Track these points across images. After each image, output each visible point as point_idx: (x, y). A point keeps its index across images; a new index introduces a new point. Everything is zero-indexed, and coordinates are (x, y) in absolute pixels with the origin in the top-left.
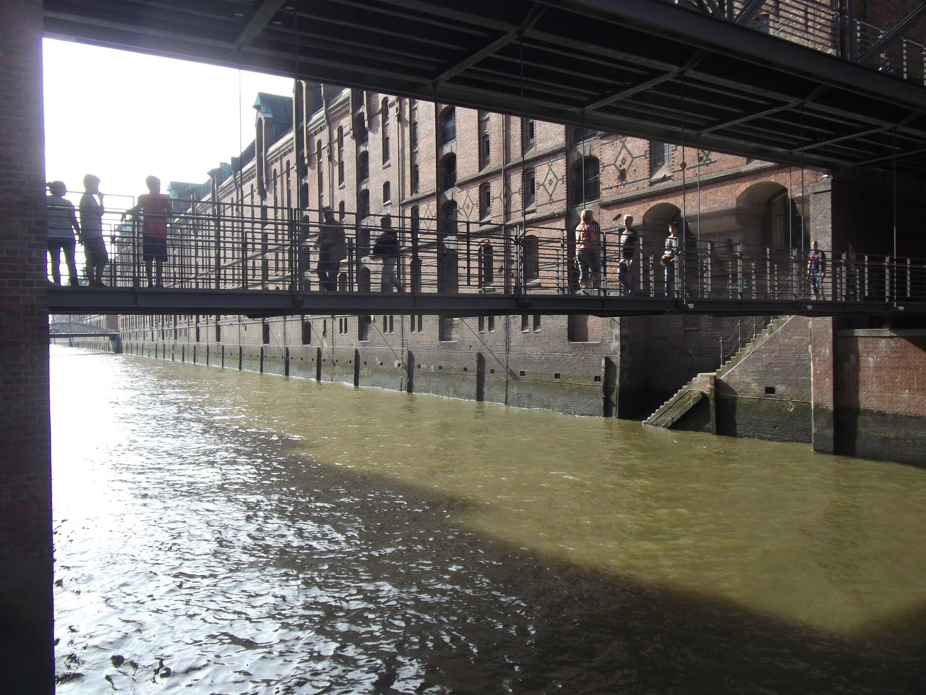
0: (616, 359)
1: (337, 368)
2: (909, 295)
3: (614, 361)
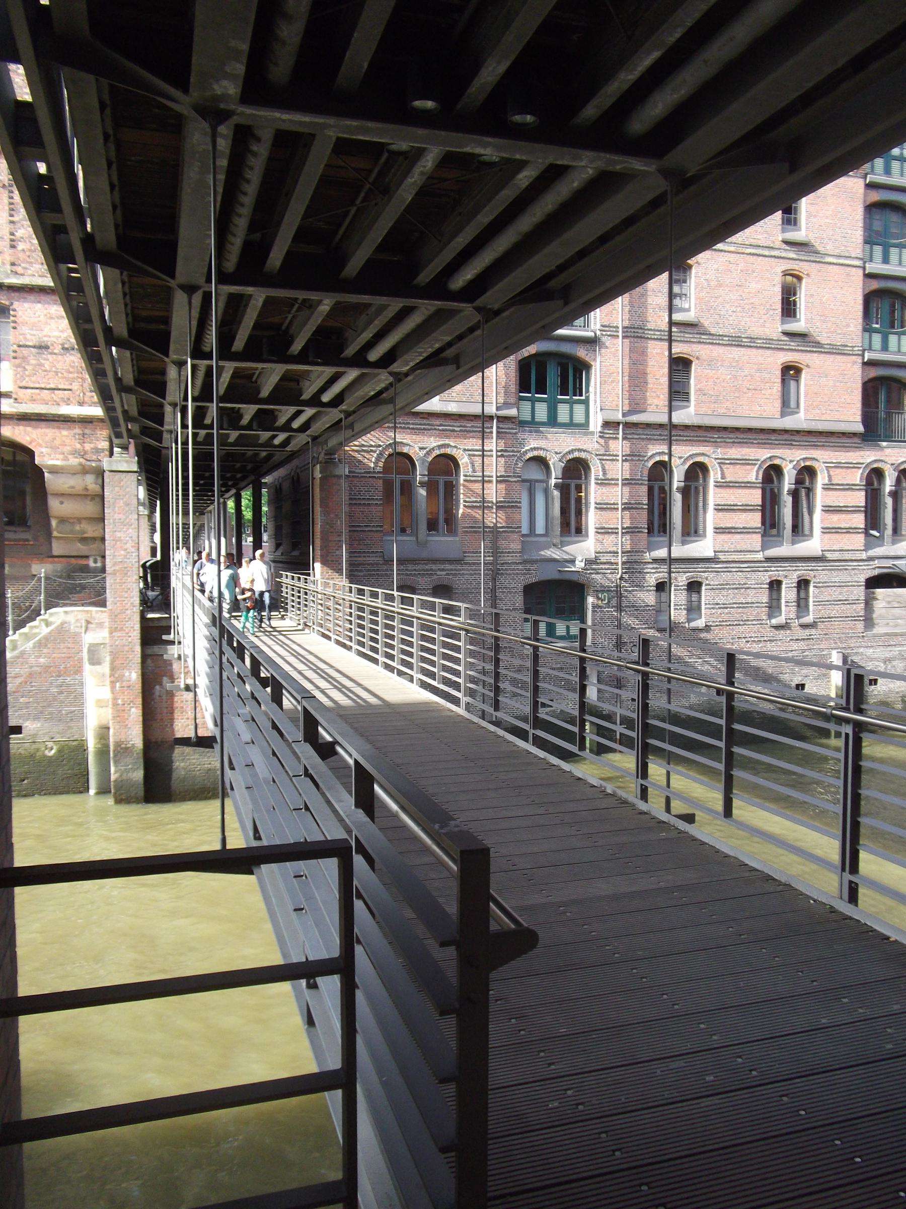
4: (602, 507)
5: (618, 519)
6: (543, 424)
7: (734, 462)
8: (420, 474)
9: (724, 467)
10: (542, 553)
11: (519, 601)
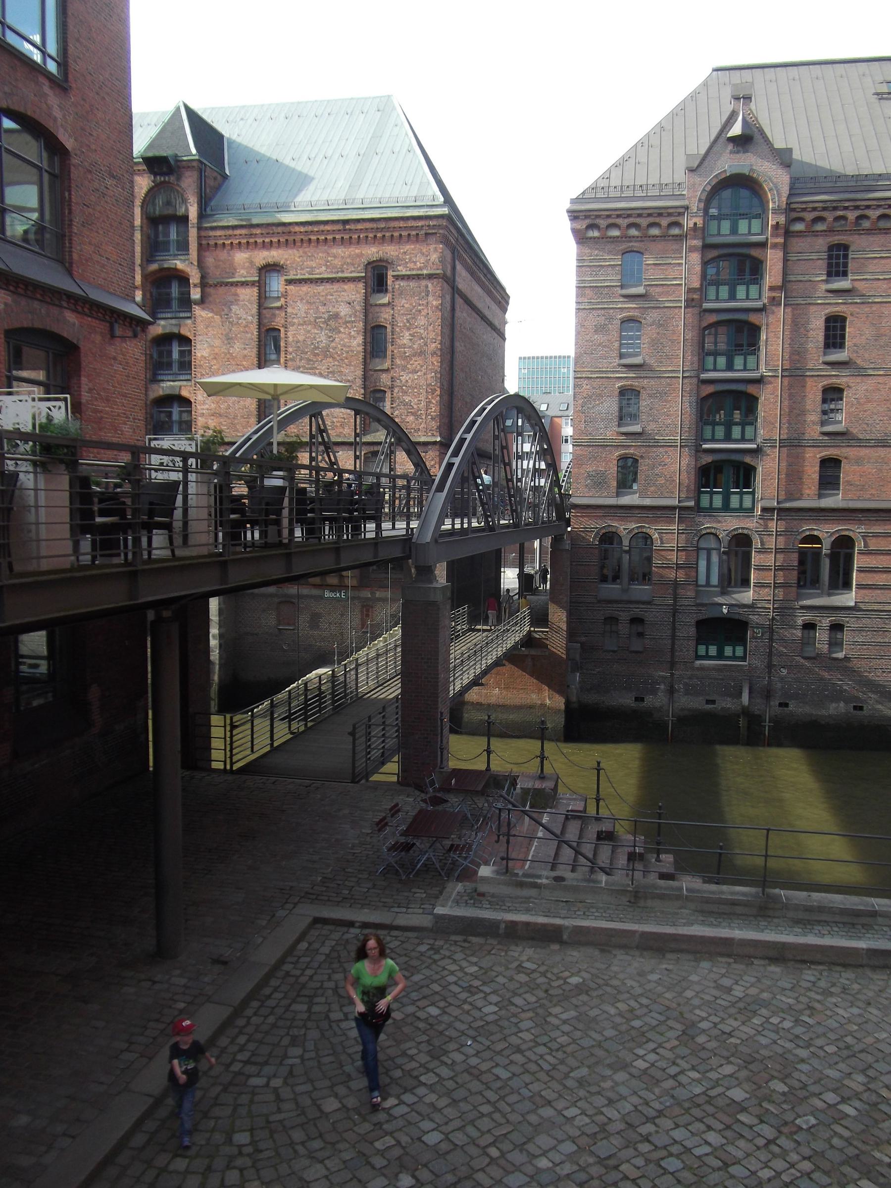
4: (760, 568)
5: (769, 578)
6: (717, 510)
7: (876, 535)
8: (626, 542)
9: (867, 539)
10: (716, 599)
11: (692, 631)
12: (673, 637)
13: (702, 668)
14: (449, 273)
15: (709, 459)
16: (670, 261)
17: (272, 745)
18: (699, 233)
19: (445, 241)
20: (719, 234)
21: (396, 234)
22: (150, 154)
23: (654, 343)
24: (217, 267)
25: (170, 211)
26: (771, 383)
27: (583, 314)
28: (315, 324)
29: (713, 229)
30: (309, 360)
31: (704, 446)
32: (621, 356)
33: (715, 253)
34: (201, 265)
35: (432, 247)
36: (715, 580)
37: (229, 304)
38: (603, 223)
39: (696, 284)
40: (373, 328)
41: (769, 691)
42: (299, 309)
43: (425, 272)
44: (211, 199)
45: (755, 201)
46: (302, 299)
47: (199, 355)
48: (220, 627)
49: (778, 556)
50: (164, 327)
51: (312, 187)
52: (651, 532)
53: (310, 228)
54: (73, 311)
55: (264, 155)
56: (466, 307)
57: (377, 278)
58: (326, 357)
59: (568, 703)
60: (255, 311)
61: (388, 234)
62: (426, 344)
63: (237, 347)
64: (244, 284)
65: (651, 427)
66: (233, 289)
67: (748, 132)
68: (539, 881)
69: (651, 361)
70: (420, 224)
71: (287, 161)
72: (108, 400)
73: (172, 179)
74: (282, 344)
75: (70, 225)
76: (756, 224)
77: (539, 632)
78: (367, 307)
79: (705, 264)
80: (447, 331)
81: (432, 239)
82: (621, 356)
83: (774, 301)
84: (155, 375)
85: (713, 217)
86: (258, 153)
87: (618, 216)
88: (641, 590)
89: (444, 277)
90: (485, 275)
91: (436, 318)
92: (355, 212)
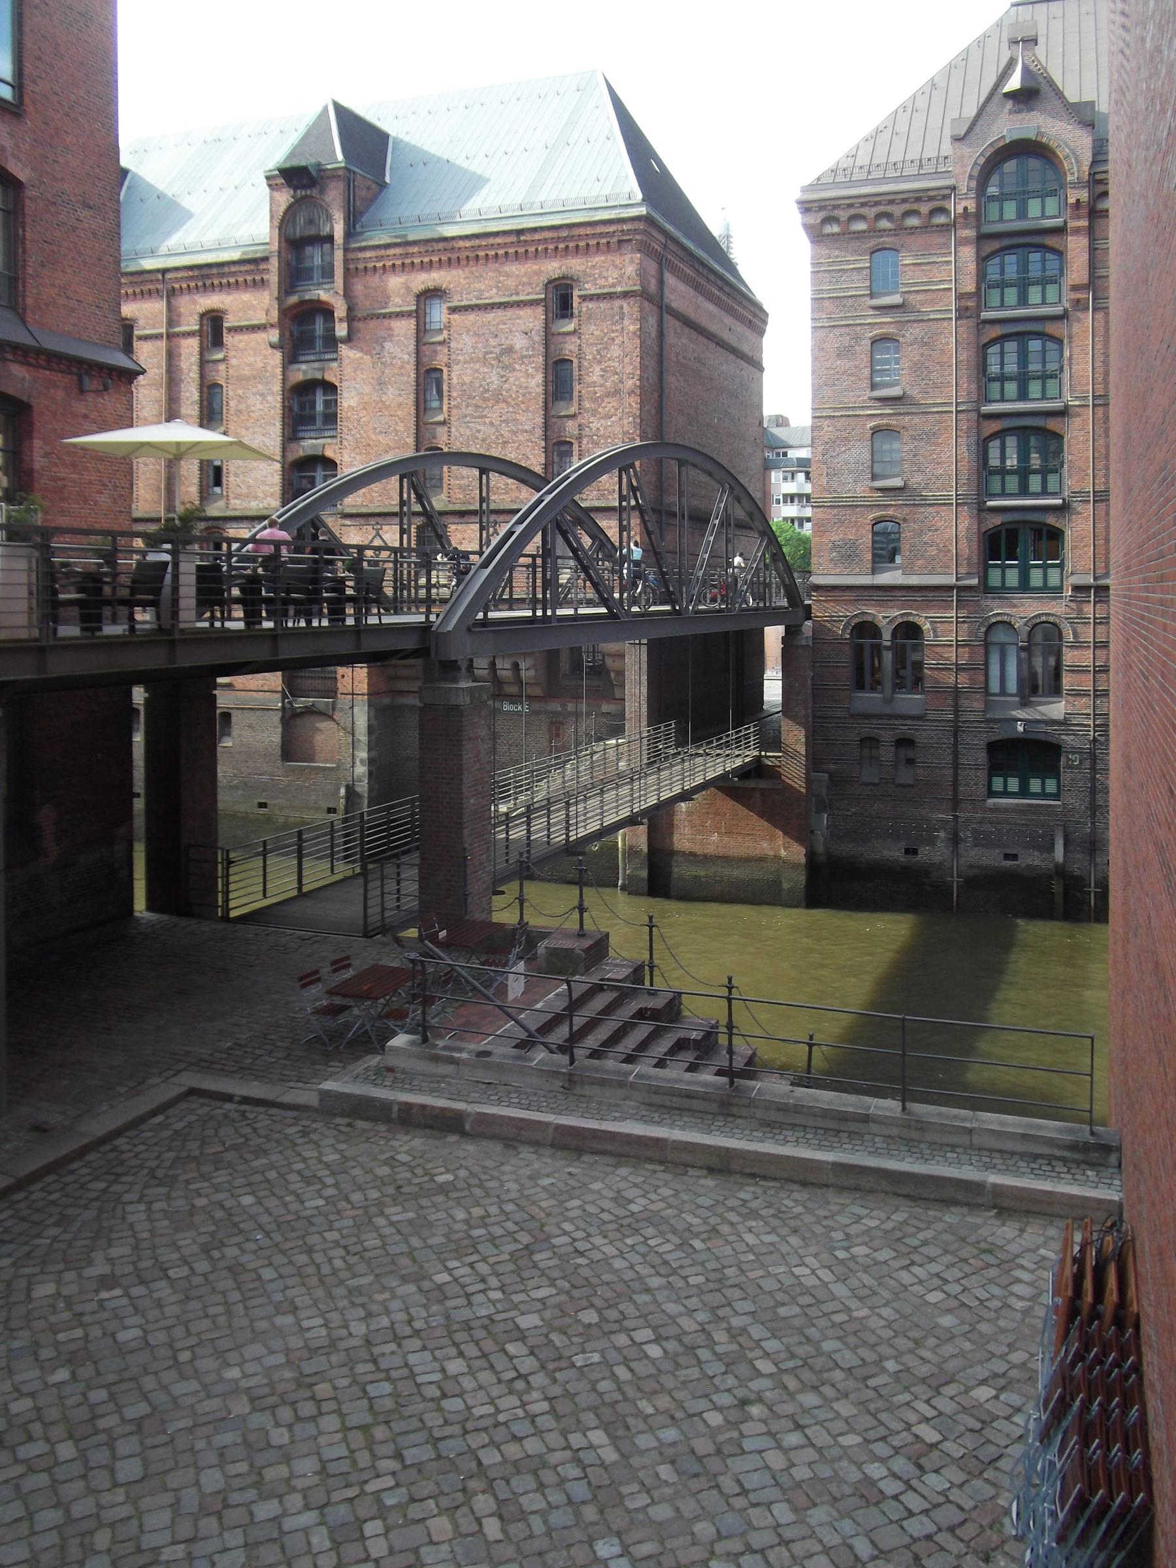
0: (363, 787)
1: (329, 294)
2: (139, 695)
3: (358, 789)
6: (1012, 590)
8: (887, 636)
11: (982, 757)
12: (956, 765)
13: (996, 809)
14: (653, 287)
15: (996, 520)
16: (935, 259)
17: (300, 889)
18: (972, 220)
19: (645, 249)
20: (1001, 220)
21: (582, 244)
22: (287, 165)
23: (917, 367)
24: (366, 296)
25: (312, 232)
26: (1079, 415)
27: (821, 334)
28: (485, 361)
29: (993, 213)
30: (477, 406)
31: (989, 503)
32: (873, 386)
33: (996, 245)
34: (348, 294)
35: (627, 258)
36: (1012, 687)
37: (381, 341)
38: (843, 215)
39: (969, 286)
40: (557, 363)
41: (1093, 843)
42: (464, 343)
43: (619, 289)
44: (362, 214)
45: (1050, 174)
46: (468, 331)
47: (345, 405)
48: (370, 750)
49: (1098, 652)
50: (305, 372)
51: (484, 192)
52: (920, 621)
53: (477, 242)
54: (22, 363)
55: (434, 156)
56: (687, 330)
57: (561, 299)
58: (497, 402)
59: (811, 855)
60: (412, 348)
61: (571, 245)
62: (621, 381)
63: (391, 395)
64: (399, 315)
65: (916, 480)
66: (386, 322)
67: (1031, 84)
68: (457, 1055)
69: (914, 392)
70: (611, 229)
71: (461, 162)
72: (74, 465)
73: (315, 192)
74: (445, 388)
75: (24, 266)
76: (1052, 205)
77: (771, 757)
78: (549, 336)
79: (982, 260)
80: (652, 363)
81: (627, 248)
82: (873, 386)
83: (1079, 305)
84: (295, 431)
85: (992, 198)
86: (427, 153)
87: (863, 205)
88: (910, 701)
89: (644, 295)
90: (720, 289)
91: (634, 346)
92: (532, 219)
